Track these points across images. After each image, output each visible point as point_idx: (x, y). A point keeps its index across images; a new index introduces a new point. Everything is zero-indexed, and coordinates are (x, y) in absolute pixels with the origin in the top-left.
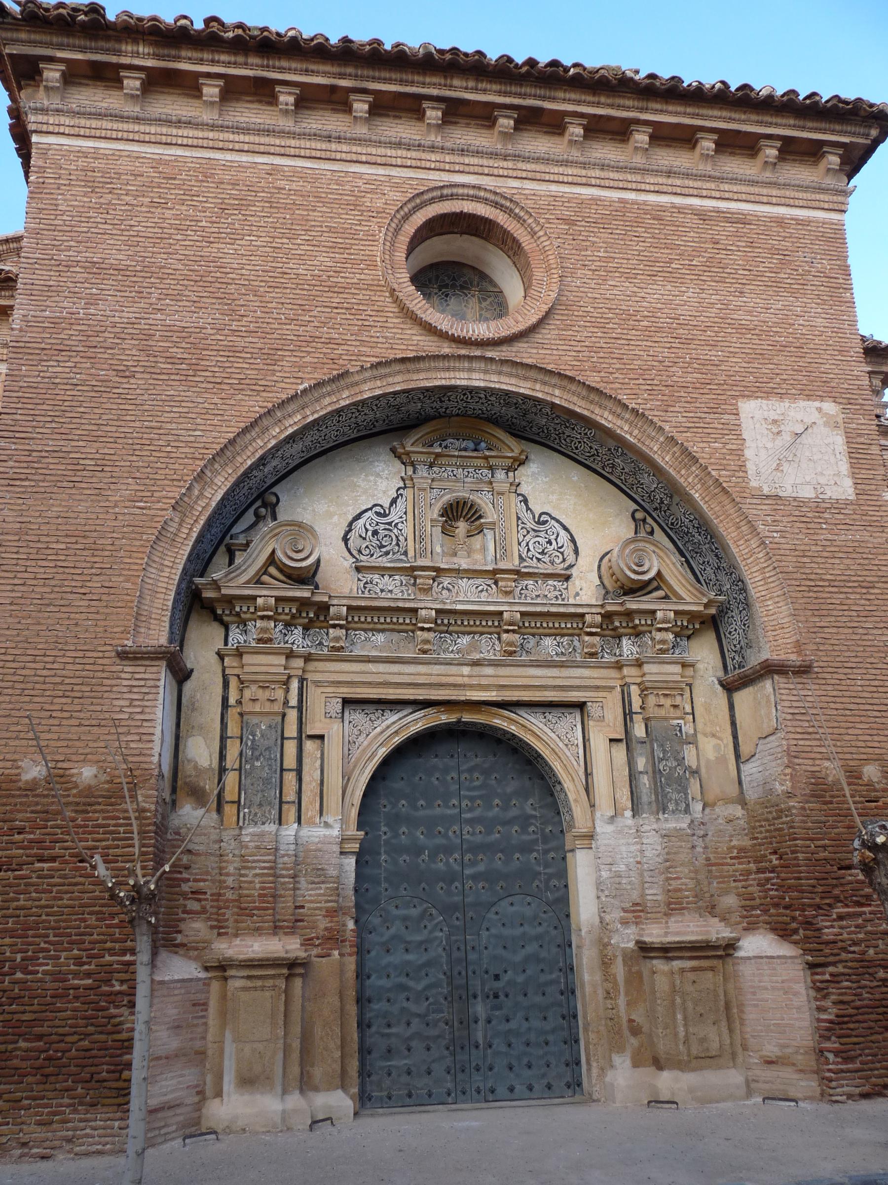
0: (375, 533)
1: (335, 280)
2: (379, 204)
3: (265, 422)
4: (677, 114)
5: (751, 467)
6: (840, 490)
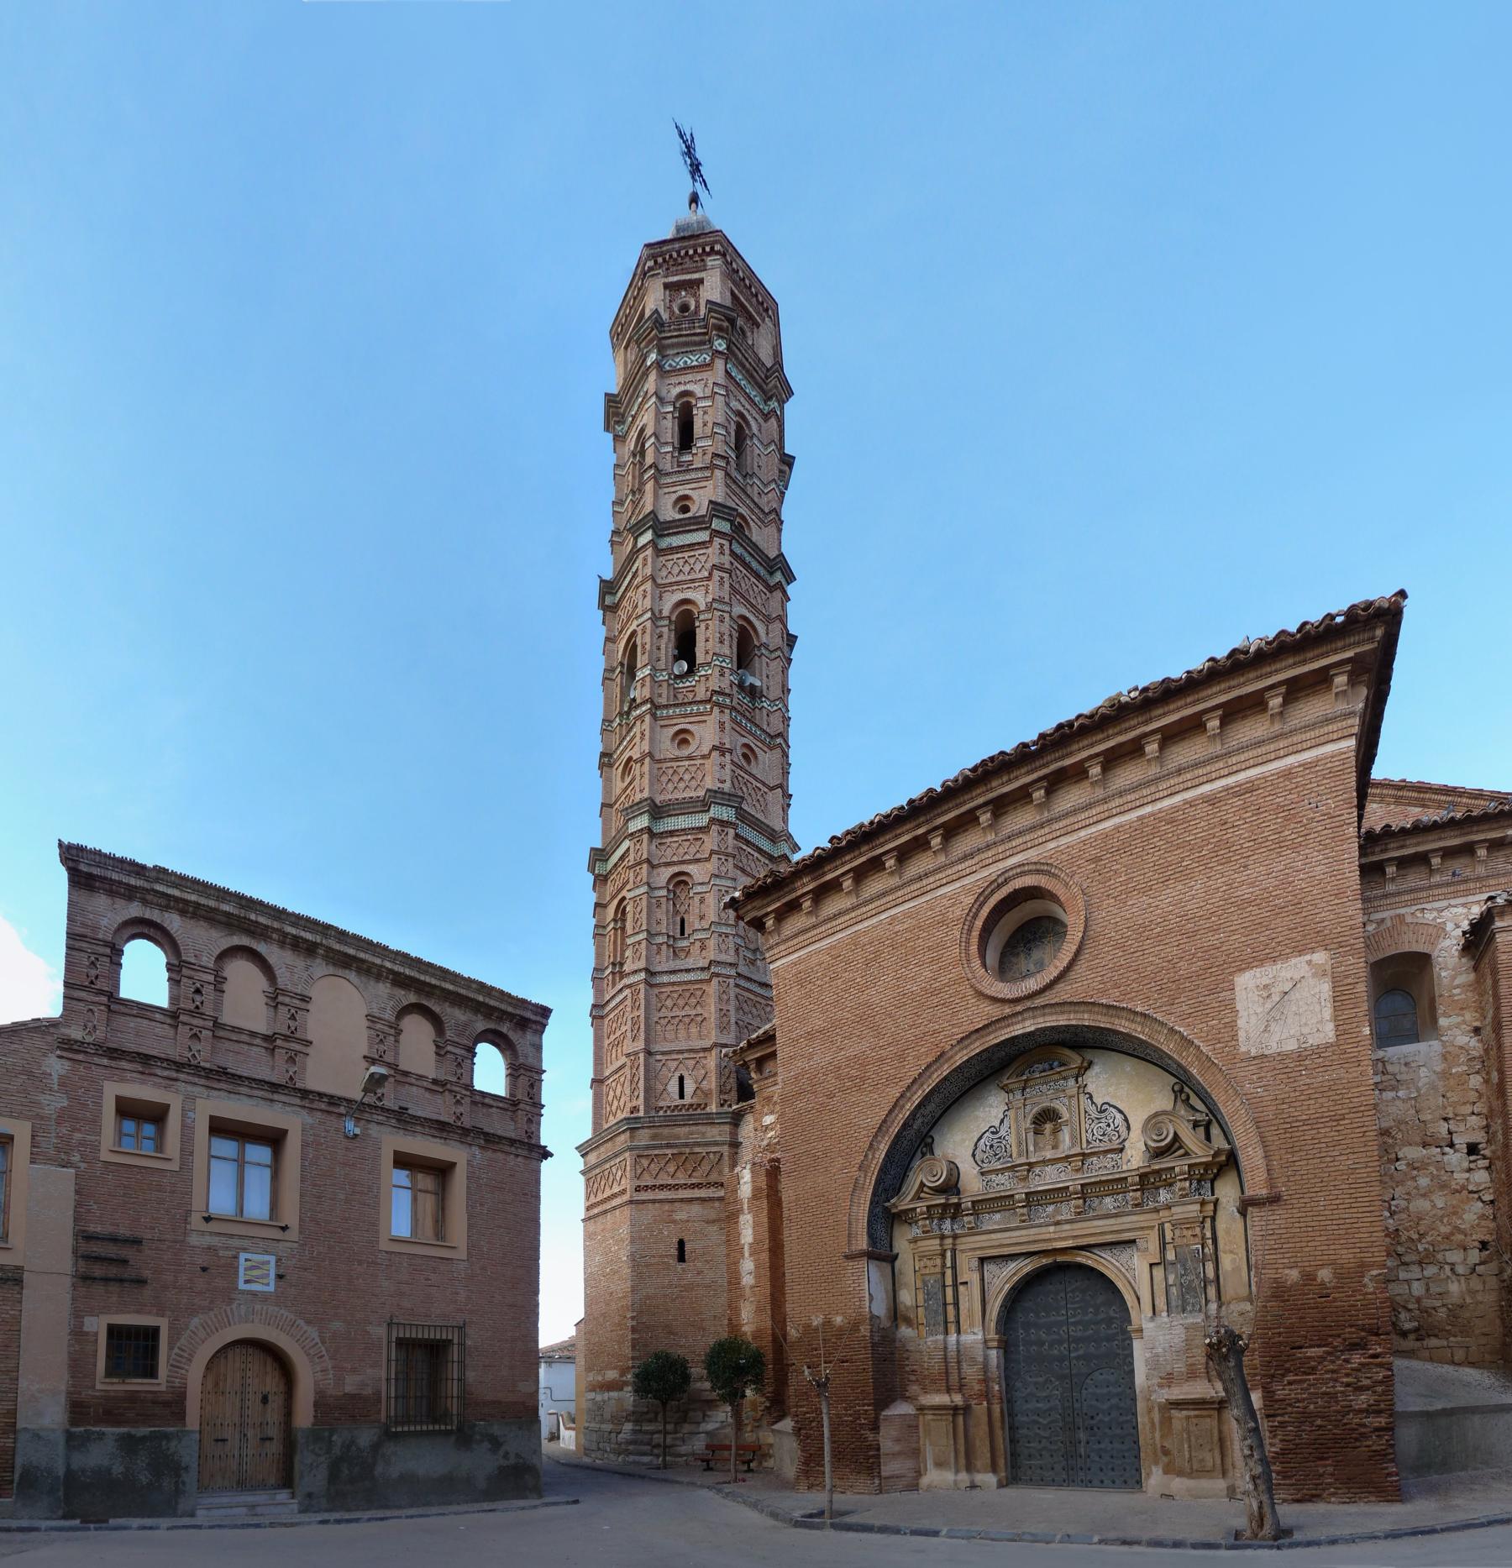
4: (1178, 709)
5: (1242, 1035)
6: (1322, 1035)
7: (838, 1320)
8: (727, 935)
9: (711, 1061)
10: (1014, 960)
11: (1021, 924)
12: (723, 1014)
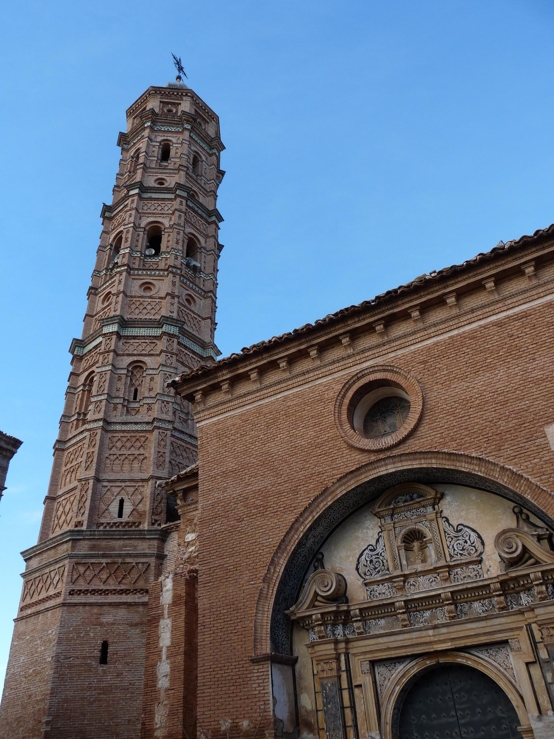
0: (371, 561)
1: (318, 441)
2: (331, 395)
3: (296, 526)
4: (465, 280)
7: (245, 724)
8: (168, 402)
9: (148, 490)
10: (375, 424)
11: (377, 402)
12: (160, 455)
